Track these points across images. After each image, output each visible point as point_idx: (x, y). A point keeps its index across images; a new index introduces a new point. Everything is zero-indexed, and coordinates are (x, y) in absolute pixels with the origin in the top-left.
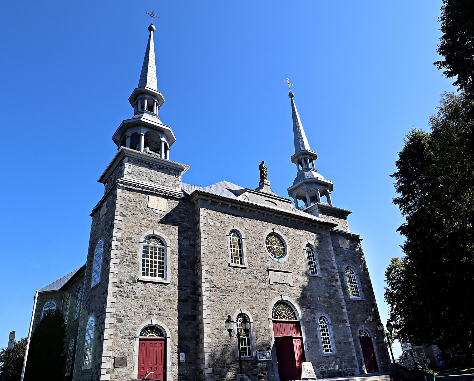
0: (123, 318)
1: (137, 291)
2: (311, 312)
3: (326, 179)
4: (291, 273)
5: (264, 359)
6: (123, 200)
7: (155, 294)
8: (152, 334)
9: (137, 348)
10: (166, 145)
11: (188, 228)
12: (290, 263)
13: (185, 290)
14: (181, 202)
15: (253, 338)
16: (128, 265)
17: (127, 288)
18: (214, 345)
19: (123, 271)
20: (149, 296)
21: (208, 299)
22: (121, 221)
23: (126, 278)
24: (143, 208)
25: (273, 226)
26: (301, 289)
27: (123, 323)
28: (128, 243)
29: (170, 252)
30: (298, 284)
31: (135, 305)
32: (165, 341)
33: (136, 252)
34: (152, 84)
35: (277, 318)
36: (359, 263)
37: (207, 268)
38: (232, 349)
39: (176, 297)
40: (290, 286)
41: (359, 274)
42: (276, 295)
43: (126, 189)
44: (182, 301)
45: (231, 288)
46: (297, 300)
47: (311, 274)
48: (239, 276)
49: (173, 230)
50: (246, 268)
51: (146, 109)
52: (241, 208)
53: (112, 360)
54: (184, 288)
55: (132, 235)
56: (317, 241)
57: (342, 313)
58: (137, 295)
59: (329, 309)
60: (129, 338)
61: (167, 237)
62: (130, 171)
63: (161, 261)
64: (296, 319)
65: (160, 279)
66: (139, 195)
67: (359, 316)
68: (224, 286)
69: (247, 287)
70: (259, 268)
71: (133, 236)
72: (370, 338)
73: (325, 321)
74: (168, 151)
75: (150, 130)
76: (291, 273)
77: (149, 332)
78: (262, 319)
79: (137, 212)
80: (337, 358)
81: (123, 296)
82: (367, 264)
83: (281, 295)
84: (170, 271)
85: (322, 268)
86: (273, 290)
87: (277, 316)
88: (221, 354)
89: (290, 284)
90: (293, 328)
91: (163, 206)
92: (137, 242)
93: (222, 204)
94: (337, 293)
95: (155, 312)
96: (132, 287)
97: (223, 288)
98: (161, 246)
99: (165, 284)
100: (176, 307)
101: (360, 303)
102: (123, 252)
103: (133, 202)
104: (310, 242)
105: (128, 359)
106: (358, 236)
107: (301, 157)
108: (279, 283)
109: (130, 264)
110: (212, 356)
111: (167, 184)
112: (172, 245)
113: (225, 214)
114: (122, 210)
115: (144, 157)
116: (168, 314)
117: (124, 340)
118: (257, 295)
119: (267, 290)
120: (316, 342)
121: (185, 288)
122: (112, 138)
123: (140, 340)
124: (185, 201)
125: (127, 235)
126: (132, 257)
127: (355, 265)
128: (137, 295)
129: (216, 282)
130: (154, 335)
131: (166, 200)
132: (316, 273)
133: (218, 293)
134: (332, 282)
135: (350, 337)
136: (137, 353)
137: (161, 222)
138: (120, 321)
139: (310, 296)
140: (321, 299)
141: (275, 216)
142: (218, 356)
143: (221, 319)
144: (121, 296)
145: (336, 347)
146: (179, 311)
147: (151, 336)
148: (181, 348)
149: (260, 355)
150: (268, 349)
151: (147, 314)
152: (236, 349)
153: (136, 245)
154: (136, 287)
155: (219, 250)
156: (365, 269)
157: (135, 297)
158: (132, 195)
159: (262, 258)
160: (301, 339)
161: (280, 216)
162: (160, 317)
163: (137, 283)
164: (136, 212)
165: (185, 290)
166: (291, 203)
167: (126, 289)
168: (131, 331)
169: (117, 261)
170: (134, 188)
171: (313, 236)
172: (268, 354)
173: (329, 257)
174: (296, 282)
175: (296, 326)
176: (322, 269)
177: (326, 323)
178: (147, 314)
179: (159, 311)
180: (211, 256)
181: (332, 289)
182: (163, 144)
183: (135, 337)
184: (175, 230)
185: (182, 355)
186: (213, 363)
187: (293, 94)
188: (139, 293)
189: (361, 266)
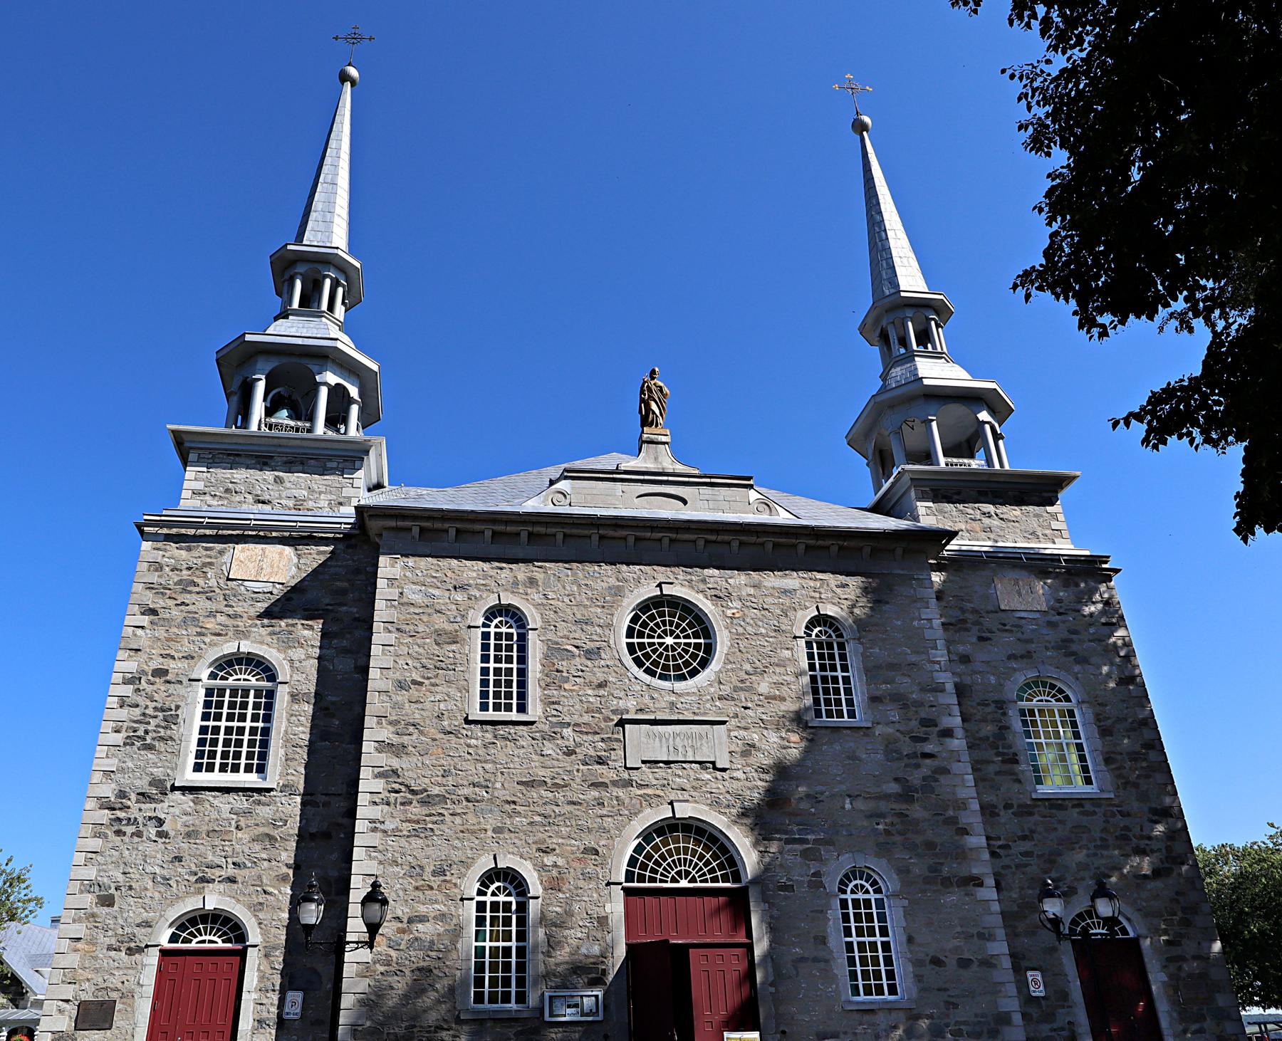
0: (117, 894)
1: (169, 818)
2: (805, 854)
3: (975, 376)
4: (724, 723)
5: (569, 1015)
6: (156, 570)
7: (225, 823)
8: (207, 938)
9: (149, 978)
10: (993, 428)
11: (356, 619)
12: (726, 690)
13: (326, 804)
14: (341, 546)
15: (536, 946)
16: (150, 748)
17: (138, 810)
18: (382, 969)
19: (130, 764)
20: (205, 828)
21: (374, 830)
22: (142, 627)
23: (138, 783)
24: (213, 583)
25: (662, 573)
26: (767, 777)
27: (116, 907)
28: (155, 687)
29: (287, 698)
30: (752, 760)
31: (159, 856)
32: (242, 954)
33: (178, 707)
34: (911, 280)
35: (652, 880)
36: (1094, 660)
37: (386, 734)
38: (446, 982)
39: (294, 826)
40: (715, 768)
41: (1096, 702)
42: (649, 800)
43: (168, 538)
44: (313, 836)
45: (467, 791)
46: (744, 813)
47: (816, 722)
48: (502, 752)
49: (306, 633)
50: (532, 723)
51: (915, 347)
52: (530, 534)
53: (72, 1010)
54: (321, 799)
55: (171, 661)
56: (863, 601)
57: (962, 854)
58: (165, 827)
59: (898, 838)
60: (129, 949)
61: (282, 656)
62: (199, 486)
63: (260, 724)
64: (737, 878)
65: (252, 779)
66: (206, 549)
67: (1080, 856)
68: (439, 785)
69: (529, 784)
70: (587, 718)
71: (172, 665)
72: (1135, 942)
73: (874, 883)
74: (1001, 442)
75: (285, 360)
76: (724, 723)
77: (199, 930)
78: (581, 883)
79: (194, 596)
80: (917, 1017)
81: (124, 834)
82: (1140, 659)
83: (671, 803)
84: (282, 752)
85: (878, 693)
86: (640, 786)
87: (654, 871)
88: (405, 997)
89: (713, 763)
90: (718, 911)
91: (280, 567)
92: (185, 681)
93: (458, 531)
94: (943, 779)
95: (217, 872)
96: (153, 806)
97: (436, 790)
98: (265, 683)
99: (259, 791)
100: (288, 856)
101: (1088, 807)
102: (137, 711)
103: (185, 572)
104: (830, 610)
105: (118, 1006)
106: (1105, 559)
107: (884, 322)
108: (667, 763)
109: (156, 743)
110: (369, 1003)
111: (311, 504)
112: (295, 677)
113: (468, 563)
114: (150, 599)
115: (241, 441)
116: (260, 877)
117: (113, 953)
118: (571, 808)
119: (611, 788)
120: (816, 960)
121: (327, 799)
122: (845, 441)
123: (164, 953)
124: (353, 541)
125: (154, 665)
126: (163, 724)
127: (1077, 668)
128: (165, 827)
129: (410, 777)
130: (215, 938)
131: (288, 550)
132: (852, 714)
133: (416, 810)
134: (925, 740)
135: (992, 938)
136: (150, 990)
137: (268, 614)
138: (107, 901)
139: (808, 796)
140: (860, 805)
141: (671, 540)
142: (390, 1003)
143: (417, 888)
144: (119, 833)
145: (919, 978)
146: (297, 867)
147: (204, 942)
148: (291, 978)
149: (557, 1003)
150: (594, 983)
151: (193, 879)
152: (464, 982)
153: (180, 689)
154: (166, 804)
155: (436, 676)
156: (1130, 679)
157: (160, 834)
158: (183, 552)
159: (602, 685)
160: (750, 948)
161: (692, 537)
162: (235, 886)
163: (170, 796)
164: (188, 598)
165: (326, 804)
166: (751, 487)
167: (134, 813)
168: (136, 930)
169: (119, 738)
170: (191, 532)
171: (844, 586)
172: (590, 997)
173: (917, 652)
174: (745, 754)
175: (728, 905)
176: (874, 700)
177: (878, 891)
178: (193, 879)
179: (231, 871)
180: (402, 697)
181: (918, 766)
182: (987, 427)
183: (147, 946)
184: (310, 633)
185: (295, 997)
186: (368, 1024)
187: (867, 119)
188: (176, 822)
189: (1105, 669)
